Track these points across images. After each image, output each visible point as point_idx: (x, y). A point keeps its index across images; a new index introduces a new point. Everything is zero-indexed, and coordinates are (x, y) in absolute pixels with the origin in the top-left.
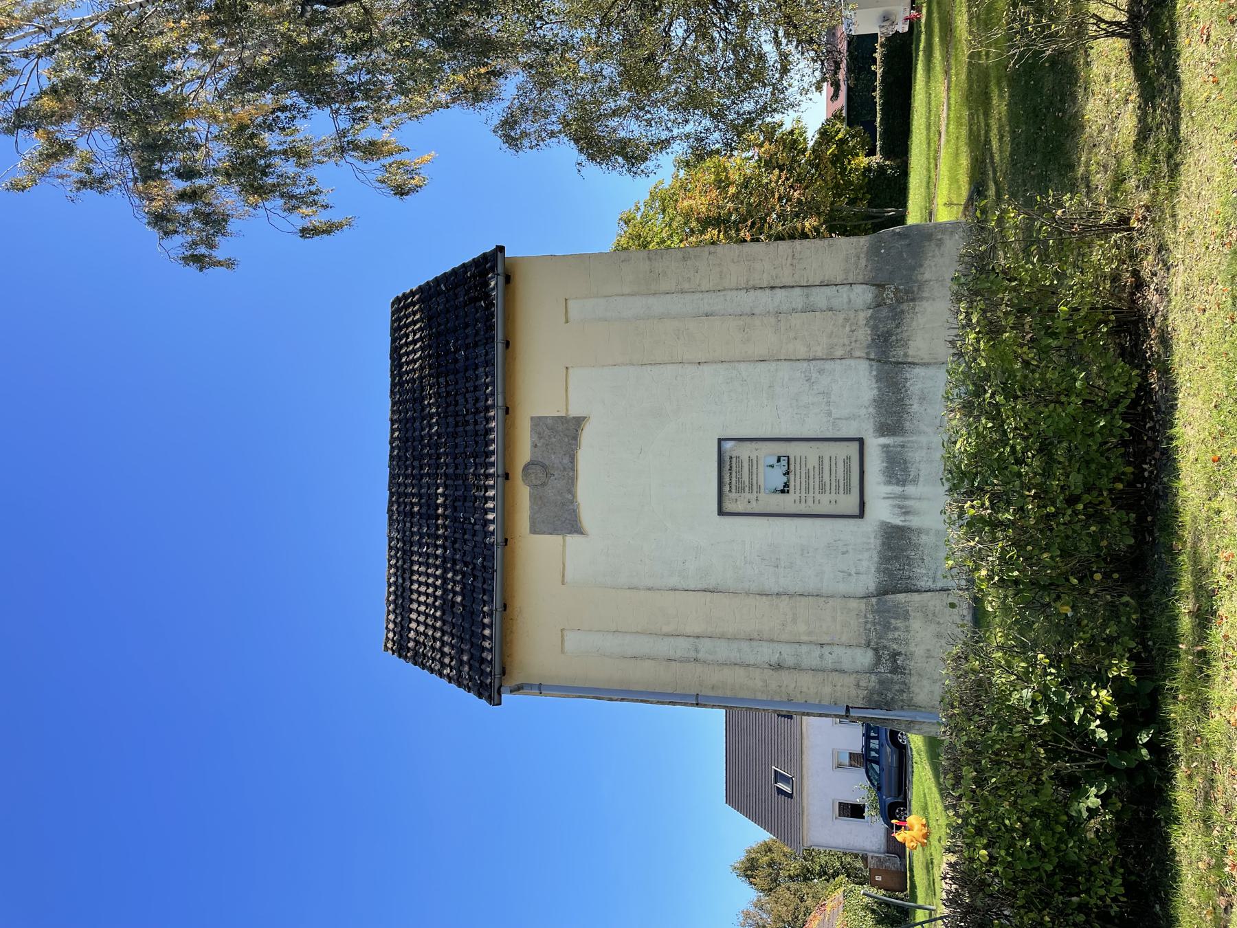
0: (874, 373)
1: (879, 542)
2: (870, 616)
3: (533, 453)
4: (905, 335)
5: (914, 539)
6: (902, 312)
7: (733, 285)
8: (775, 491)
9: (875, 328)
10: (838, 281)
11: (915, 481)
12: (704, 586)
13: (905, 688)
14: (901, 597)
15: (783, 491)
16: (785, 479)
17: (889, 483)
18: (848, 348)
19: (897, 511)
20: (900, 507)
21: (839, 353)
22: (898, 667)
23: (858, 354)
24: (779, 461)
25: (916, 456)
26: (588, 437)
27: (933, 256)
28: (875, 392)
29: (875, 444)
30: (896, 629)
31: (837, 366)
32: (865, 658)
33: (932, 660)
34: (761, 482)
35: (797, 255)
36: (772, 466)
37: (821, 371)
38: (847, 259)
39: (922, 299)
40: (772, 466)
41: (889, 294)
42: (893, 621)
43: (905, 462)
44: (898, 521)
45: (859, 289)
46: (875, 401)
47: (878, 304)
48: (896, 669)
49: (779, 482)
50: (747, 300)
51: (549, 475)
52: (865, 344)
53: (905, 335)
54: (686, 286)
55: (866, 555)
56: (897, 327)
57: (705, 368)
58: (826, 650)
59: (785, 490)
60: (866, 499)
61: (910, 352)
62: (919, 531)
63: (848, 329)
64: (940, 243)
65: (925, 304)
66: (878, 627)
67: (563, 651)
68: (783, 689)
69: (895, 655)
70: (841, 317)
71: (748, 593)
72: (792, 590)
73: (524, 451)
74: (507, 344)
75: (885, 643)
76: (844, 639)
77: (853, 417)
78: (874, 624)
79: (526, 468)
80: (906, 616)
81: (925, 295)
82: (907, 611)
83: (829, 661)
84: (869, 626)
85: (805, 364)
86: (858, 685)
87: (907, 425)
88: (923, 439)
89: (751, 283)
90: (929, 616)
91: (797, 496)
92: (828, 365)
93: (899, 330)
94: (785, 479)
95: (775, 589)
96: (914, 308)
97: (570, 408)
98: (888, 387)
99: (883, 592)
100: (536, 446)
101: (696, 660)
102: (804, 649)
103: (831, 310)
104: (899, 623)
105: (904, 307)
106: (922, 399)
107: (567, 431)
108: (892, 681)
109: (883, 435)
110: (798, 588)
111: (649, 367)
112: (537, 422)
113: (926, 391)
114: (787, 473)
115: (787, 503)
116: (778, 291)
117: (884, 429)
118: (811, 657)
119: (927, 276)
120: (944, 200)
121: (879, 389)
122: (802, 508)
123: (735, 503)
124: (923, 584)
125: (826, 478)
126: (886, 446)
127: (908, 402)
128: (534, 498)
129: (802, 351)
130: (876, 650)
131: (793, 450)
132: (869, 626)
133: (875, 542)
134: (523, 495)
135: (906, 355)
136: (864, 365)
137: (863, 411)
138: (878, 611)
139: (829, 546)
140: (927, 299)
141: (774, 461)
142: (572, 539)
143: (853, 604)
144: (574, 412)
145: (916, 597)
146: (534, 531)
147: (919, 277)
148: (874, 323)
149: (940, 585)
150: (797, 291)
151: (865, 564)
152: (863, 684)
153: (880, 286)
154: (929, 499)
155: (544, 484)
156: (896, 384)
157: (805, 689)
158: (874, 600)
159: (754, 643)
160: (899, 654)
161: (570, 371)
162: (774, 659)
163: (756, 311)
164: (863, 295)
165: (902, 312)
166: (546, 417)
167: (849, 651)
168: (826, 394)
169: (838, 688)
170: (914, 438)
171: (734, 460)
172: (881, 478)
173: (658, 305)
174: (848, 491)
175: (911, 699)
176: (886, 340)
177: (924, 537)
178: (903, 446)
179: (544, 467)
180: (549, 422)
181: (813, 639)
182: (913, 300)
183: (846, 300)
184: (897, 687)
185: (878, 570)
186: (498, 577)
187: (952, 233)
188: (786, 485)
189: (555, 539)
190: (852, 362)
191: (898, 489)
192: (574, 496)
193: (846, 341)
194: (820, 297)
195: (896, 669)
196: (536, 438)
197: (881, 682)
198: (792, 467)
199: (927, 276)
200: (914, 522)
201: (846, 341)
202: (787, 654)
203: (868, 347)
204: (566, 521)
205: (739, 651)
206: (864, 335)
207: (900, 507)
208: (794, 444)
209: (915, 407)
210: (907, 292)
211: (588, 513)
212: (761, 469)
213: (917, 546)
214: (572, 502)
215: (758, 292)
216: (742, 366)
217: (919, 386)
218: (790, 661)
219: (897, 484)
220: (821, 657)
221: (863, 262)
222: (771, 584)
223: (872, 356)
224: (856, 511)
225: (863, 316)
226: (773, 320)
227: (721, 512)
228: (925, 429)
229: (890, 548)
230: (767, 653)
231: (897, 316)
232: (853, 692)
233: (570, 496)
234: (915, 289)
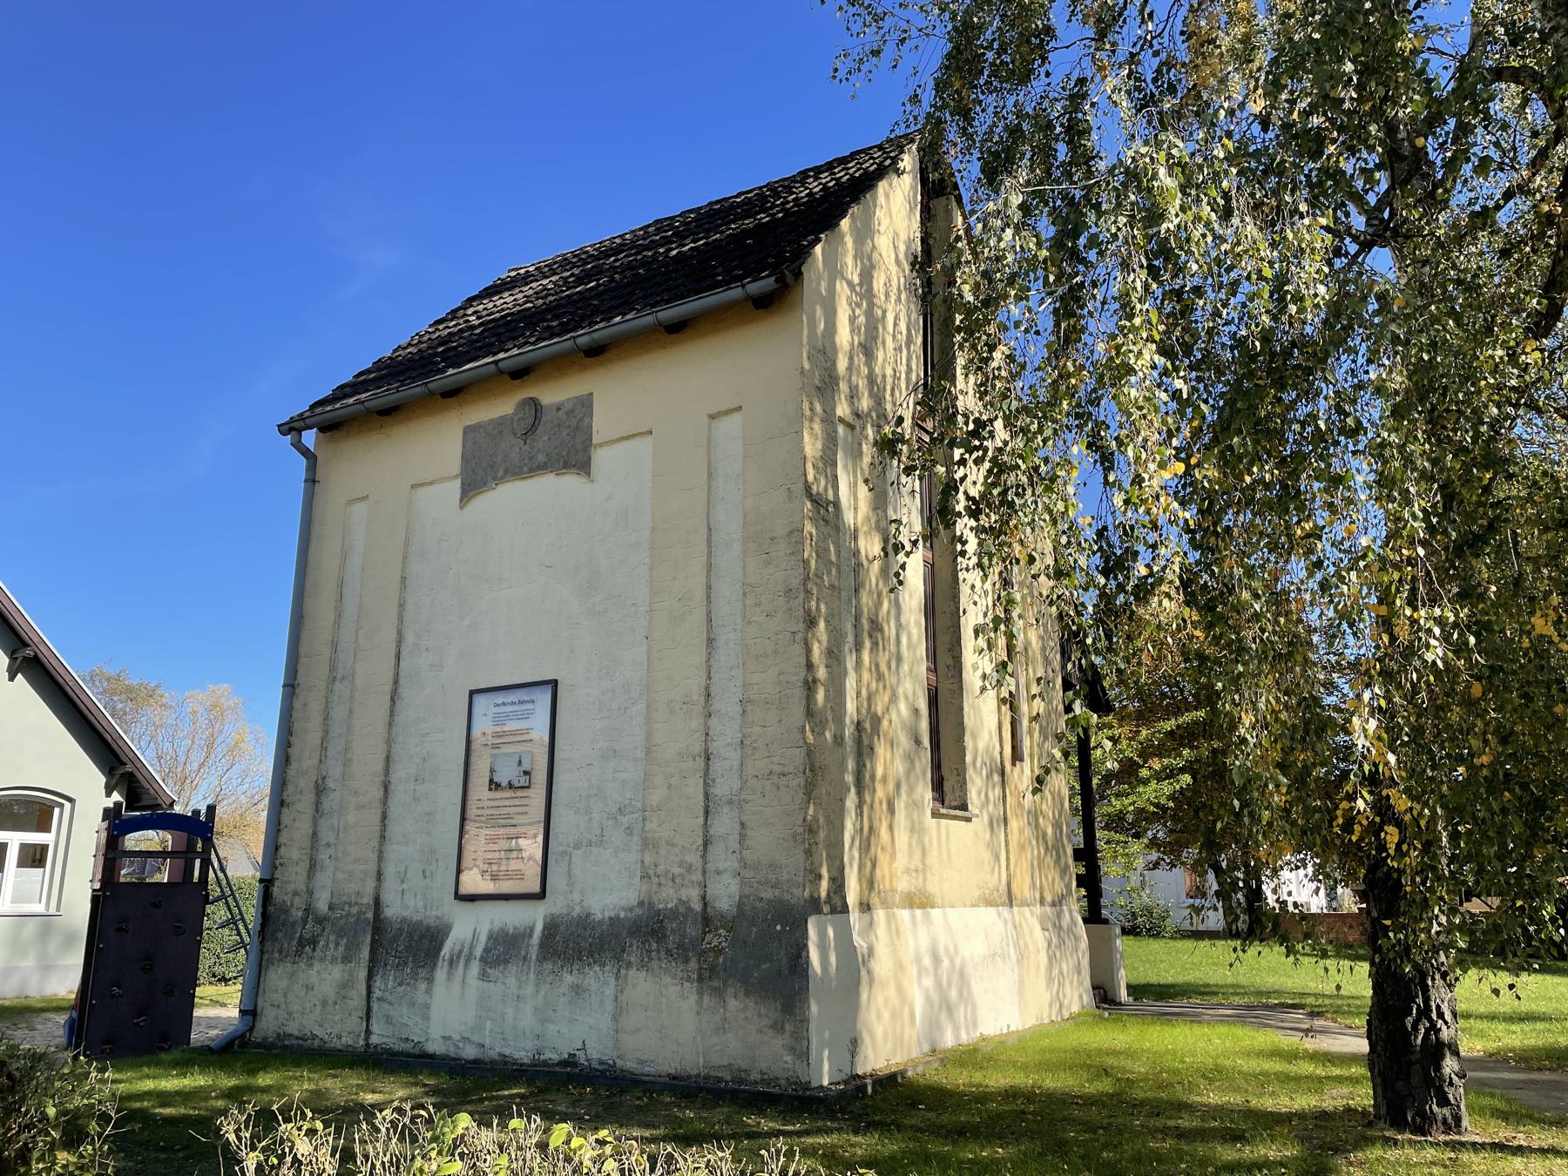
0: (622, 915)
1: (431, 922)
2: (355, 910)
5: (423, 973)
8: (492, 771)
9: (674, 914)
11: (483, 976)
12: (402, 680)
14: (365, 953)
15: (491, 781)
16: (504, 784)
18: (651, 872)
19: (458, 948)
20: (461, 952)
24: (526, 773)
25: (510, 980)
27: (760, 1015)
28: (599, 916)
30: (337, 944)
34: (506, 749)
36: (520, 762)
37: (629, 830)
38: (773, 866)
39: (700, 994)
40: (520, 762)
43: (506, 962)
44: (446, 951)
46: (588, 915)
47: (707, 920)
48: (302, 943)
52: (655, 899)
53: (655, 964)
55: (420, 904)
59: (494, 785)
60: (478, 904)
61: (632, 972)
62: (430, 980)
63: (677, 870)
64: (777, 1027)
65: (694, 998)
67: (350, 502)
69: (313, 942)
71: (389, 742)
72: (391, 801)
80: (346, 959)
81: (706, 999)
86: (295, 894)
87: (548, 966)
88: (529, 990)
93: (663, 954)
94: (504, 784)
95: (394, 778)
96: (689, 979)
97: (605, 449)
98: (601, 938)
99: (379, 924)
100: (558, 409)
101: (334, 679)
103: (706, 843)
106: (577, 990)
107: (573, 454)
108: (292, 939)
109: (545, 928)
110: (393, 812)
113: (586, 995)
114: (511, 786)
115: (479, 790)
117: (551, 927)
119: (733, 1004)
121: (601, 922)
126: (532, 929)
127: (576, 967)
128: (501, 423)
131: (537, 795)
133: (431, 916)
134: (502, 407)
139: (433, 851)
140: (699, 1002)
141: (526, 766)
143: (369, 887)
146: (468, 431)
147: (731, 990)
149: (375, 1006)
151: (411, 903)
154: (463, 995)
156: (601, 950)
158: (370, 915)
163: (714, 722)
165: (687, 961)
168: (601, 842)
170: (532, 976)
171: (530, 706)
172: (497, 925)
173: (730, 558)
177: (423, 986)
178: (525, 958)
180: (587, 420)
182: (701, 979)
183: (721, 866)
185: (404, 920)
187: (792, 1050)
188: (498, 786)
191: (478, 952)
192: (499, 480)
193: (660, 869)
196: (569, 406)
197: (293, 924)
199: (733, 1004)
200: (441, 973)
201: (660, 869)
207: (461, 952)
209: (569, 979)
212: (1025, 723)
213: (414, 976)
217: (594, 986)
219: (486, 950)
221: (767, 894)
222: (399, 773)
224: (463, 890)
225: (693, 894)
227: (554, 684)
228: (541, 994)
229: (422, 937)
230: (334, 770)
231: (681, 953)
232: (291, 888)
234: (715, 984)
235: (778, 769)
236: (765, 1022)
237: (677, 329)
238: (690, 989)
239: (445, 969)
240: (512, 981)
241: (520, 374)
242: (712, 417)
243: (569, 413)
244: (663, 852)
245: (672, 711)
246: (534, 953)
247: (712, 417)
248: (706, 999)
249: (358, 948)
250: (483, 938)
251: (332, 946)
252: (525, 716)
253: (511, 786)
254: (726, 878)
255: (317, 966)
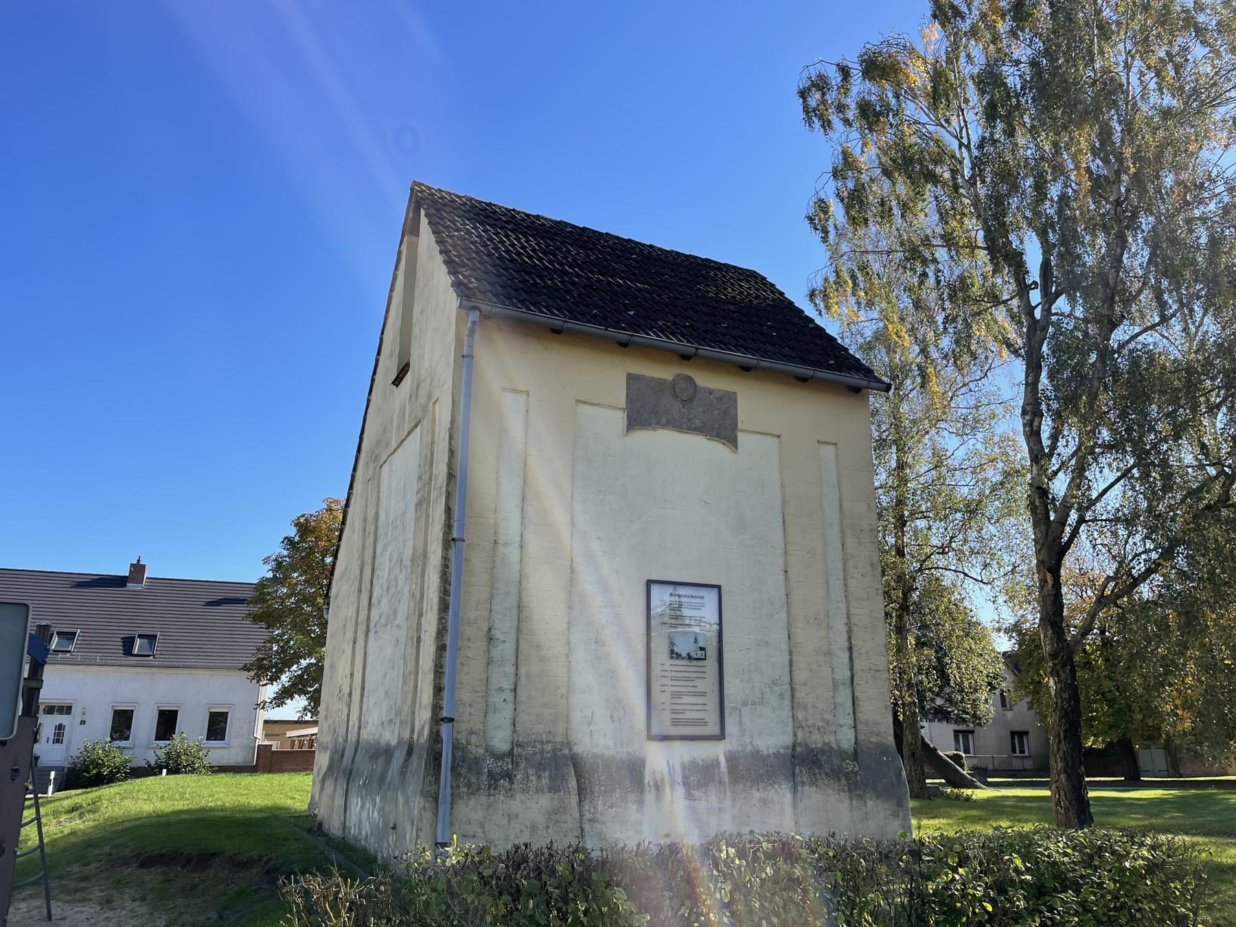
2: (549, 747)
3: (704, 389)
4: (820, 782)
6: (839, 780)
7: (853, 610)
8: (672, 644)
9: (822, 751)
10: (859, 715)
13: (474, 790)
14: (573, 783)
15: (672, 652)
16: (684, 655)
17: (684, 768)
21: (800, 715)
22: (497, 780)
23: (800, 734)
24: (702, 649)
26: (717, 449)
29: (718, 751)
30: (539, 777)
31: (786, 714)
32: (500, 740)
33: (505, 822)
35: (877, 674)
37: (781, 696)
39: (851, 799)
41: (850, 766)
42: (547, 773)
43: (706, 785)
45: (851, 734)
46: (758, 752)
47: (841, 753)
48: (494, 778)
49: (683, 649)
50: (840, 624)
51: (684, 402)
52: (808, 741)
53: (820, 782)
54: (851, 564)
56: (826, 774)
57: (782, 577)
58: (509, 695)
61: (806, 788)
62: (640, 802)
63: (820, 724)
64: (895, 815)
65: (847, 802)
66: (538, 757)
68: (466, 643)
69: (510, 777)
70: (829, 717)
73: (708, 381)
74: (557, 331)
75: (522, 765)
76: (523, 717)
77: (742, 730)
78: (542, 752)
79: (690, 379)
80: (554, 789)
81: (854, 802)
82: (559, 791)
83: (497, 699)
84: (539, 746)
85: (787, 679)
86: (471, 733)
88: (728, 804)
89: (855, 628)
90: (555, 814)
91: (667, 667)
92: (787, 703)
94: (684, 655)
102: (510, 669)
104: (545, 781)
105: (844, 781)
106: (764, 802)
107: (723, 429)
108: (479, 774)
109: (727, 761)
111: (781, 520)
112: (732, 398)
114: (690, 657)
116: (847, 655)
117: (732, 759)
118: (502, 678)
119: (870, 803)
120: (411, 804)
122: (656, 672)
123: (661, 597)
124: (587, 808)
125: (686, 700)
128: (661, 382)
129: (800, 676)
130: (510, 753)
131: (711, 663)
132: (539, 746)
134: (664, 372)
135: (803, 784)
136: (787, 740)
137: (748, 740)
138: (555, 755)
140: (851, 804)
141: (701, 644)
142: (620, 418)
144: (741, 437)
145: (574, 800)
146: (630, 377)
148: (827, 750)
150: (848, 674)
152: (474, 739)
153: (855, 756)
155: (675, 396)
157: (466, 669)
159: (515, 612)
160: (511, 782)
161: (776, 440)
162: (497, 634)
164: (846, 739)
165: (839, 780)
166: (736, 408)
167: (508, 723)
168: (762, 702)
169: (469, 710)
171: (699, 600)
172: (687, 758)
174: (675, 722)
175: (461, 798)
176: (814, 763)
178: (720, 782)
179: (691, 400)
181: (523, 681)
182: (850, 790)
183: (842, 722)
184: (473, 780)
186: (599, 330)
188: (679, 656)
189: (622, 402)
190: (790, 729)
191: (679, 777)
192: (665, 426)
193: (810, 722)
194: (844, 696)
195: (494, 778)
198: (694, 663)
199: (870, 803)
201: (810, 722)
202: (505, 649)
203: (806, 745)
204: (643, 412)
205: (506, 594)
206: (816, 740)
208: (716, 665)
209: (757, 795)
210: (855, 783)
211: (644, 437)
214: (658, 423)
215: (845, 636)
216: (783, 616)
218: (496, 653)
219: (684, 777)
220: (501, 690)
221: (874, 739)
223: (798, 749)
225: (830, 738)
226: (825, 649)
227: (649, 583)
231: (836, 774)
233: (663, 422)
235: (874, 667)
236: (889, 812)
237: (803, 380)
238: (845, 797)
239: (653, 792)
240: (713, 798)
241: (686, 357)
242: (578, 401)
243: (719, 399)
244: (810, 712)
245: (808, 623)
246: (726, 779)
247: (578, 401)
248: (854, 802)
249: (564, 779)
250: (678, 768)
251: (533, 778)
252: (698, 607)
253: (690, 657)
254: (845, 729)
255: (519, 797)
